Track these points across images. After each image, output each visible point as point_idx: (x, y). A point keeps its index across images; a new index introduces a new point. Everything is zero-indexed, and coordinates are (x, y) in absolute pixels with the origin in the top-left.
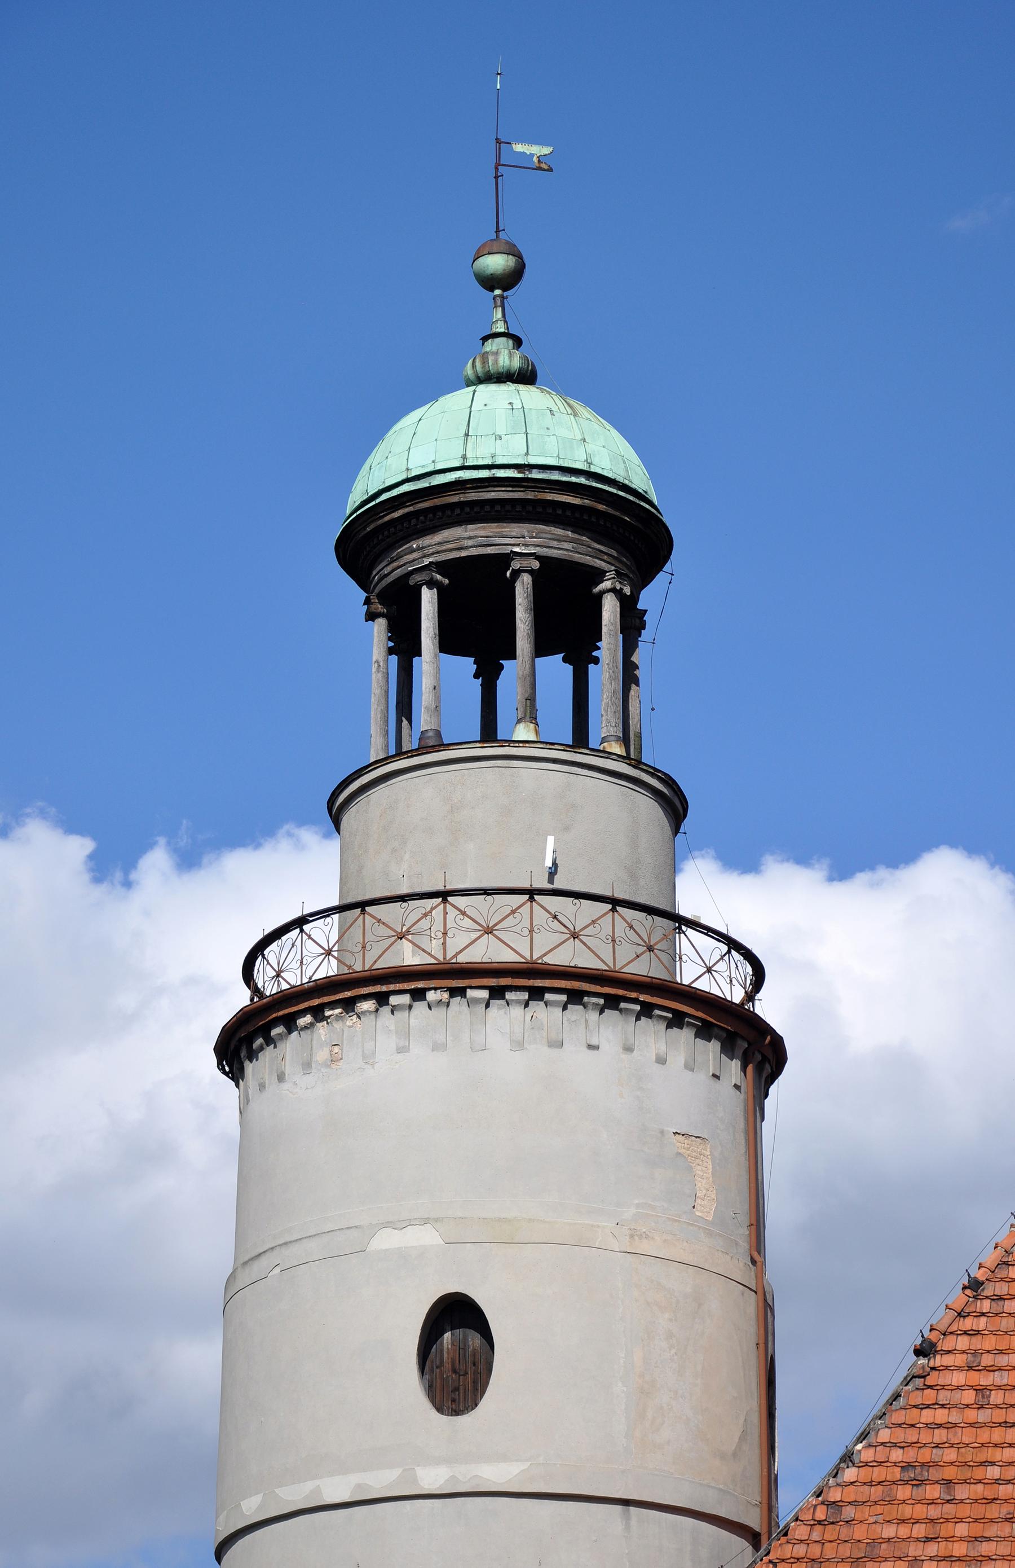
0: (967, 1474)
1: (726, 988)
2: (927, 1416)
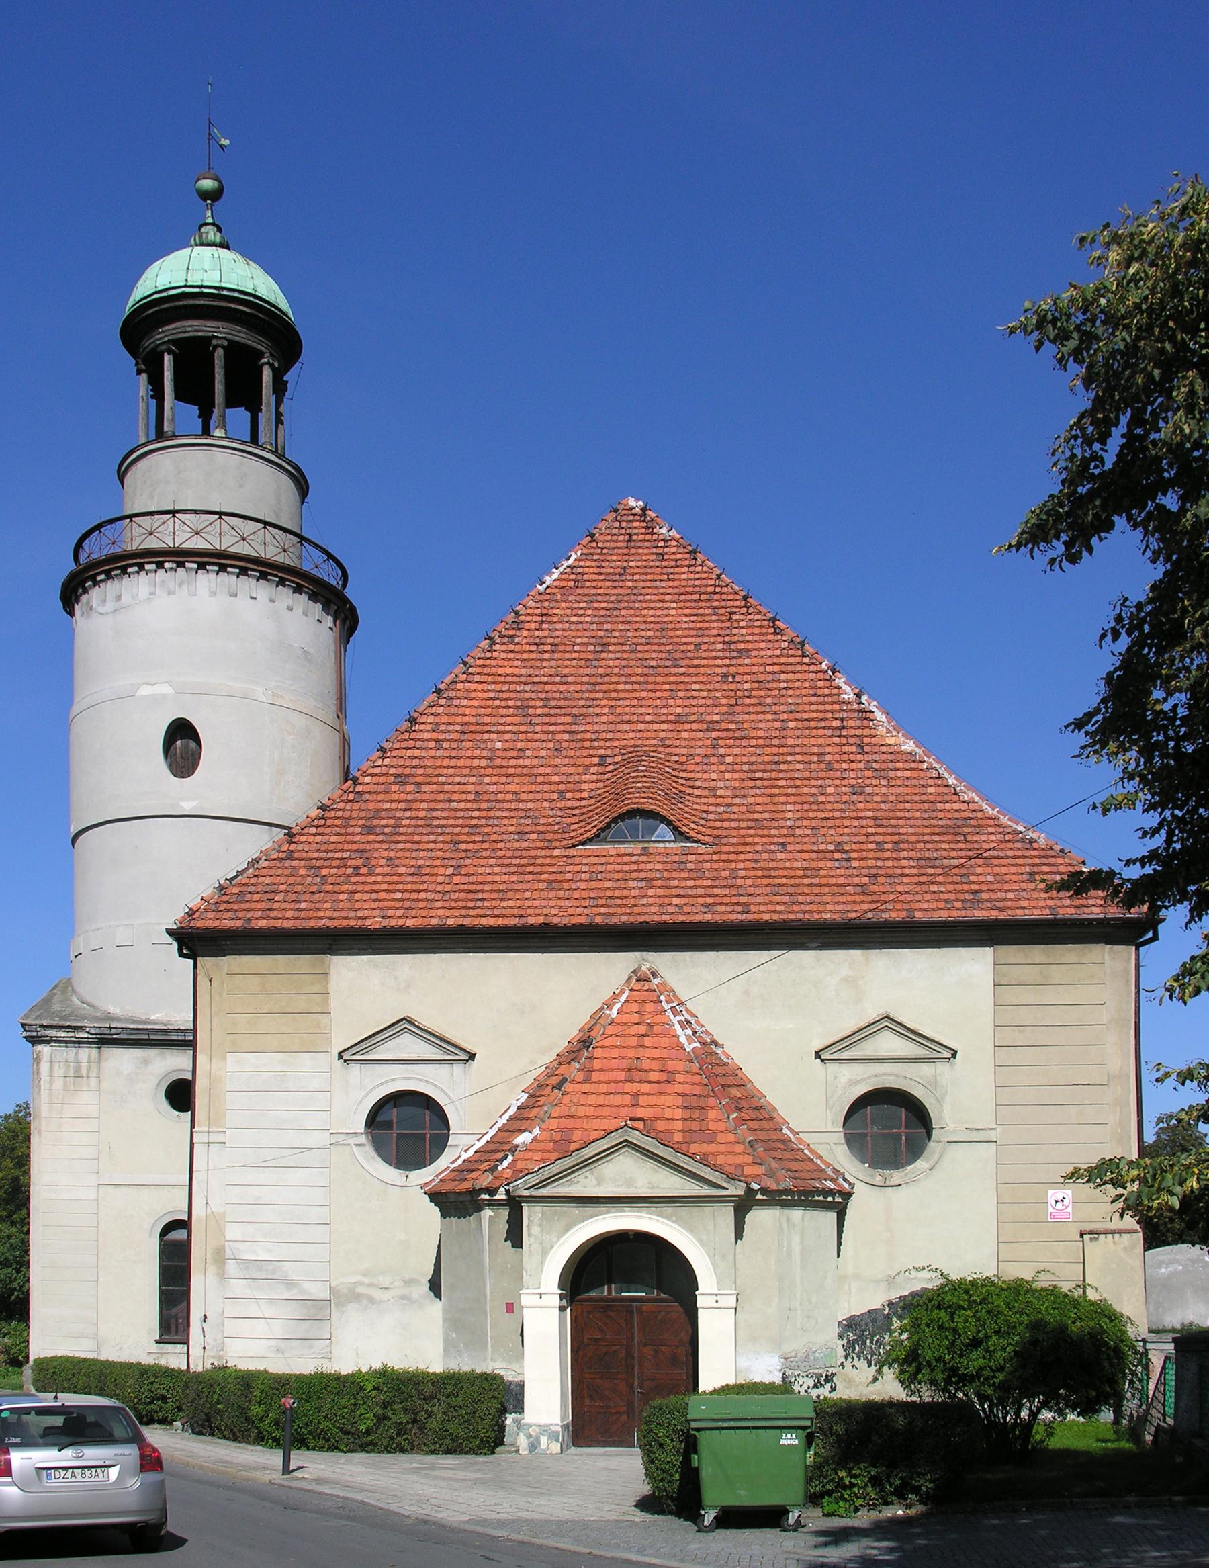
0: (428, 779)
2: (410, 753)
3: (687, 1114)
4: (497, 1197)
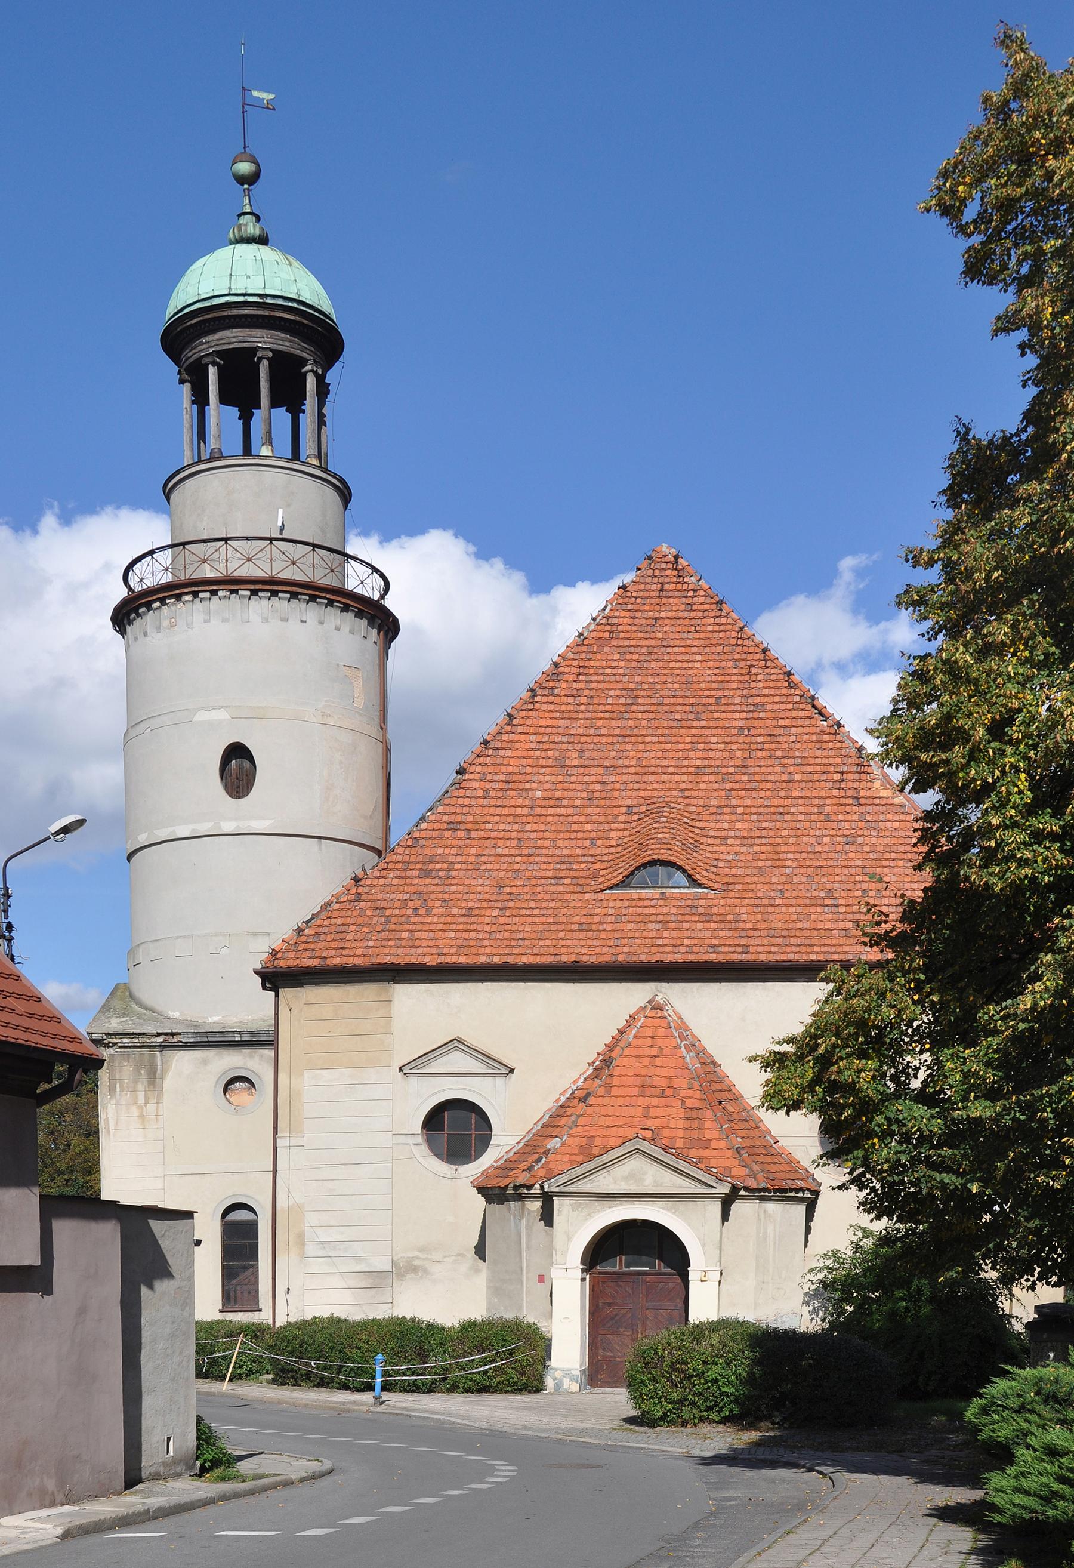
1: (370, 592)
2: (460, 801)
3: (688, 1124)
4: (532, 1191)
